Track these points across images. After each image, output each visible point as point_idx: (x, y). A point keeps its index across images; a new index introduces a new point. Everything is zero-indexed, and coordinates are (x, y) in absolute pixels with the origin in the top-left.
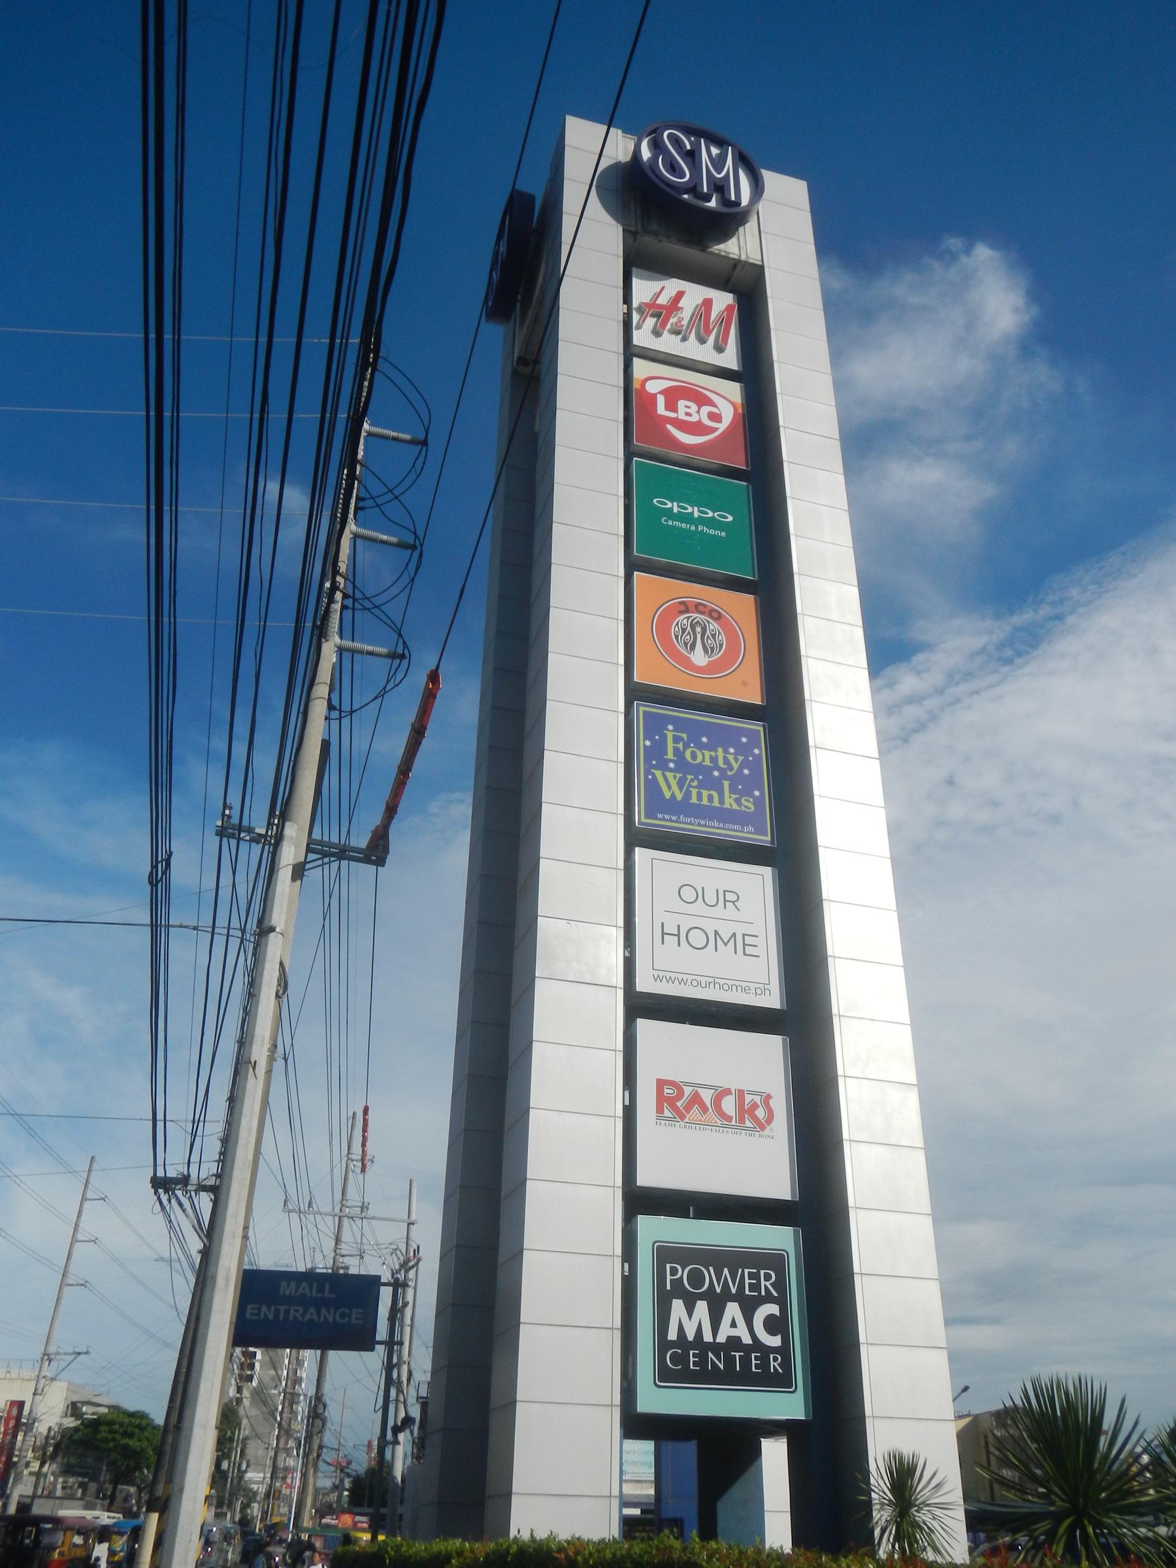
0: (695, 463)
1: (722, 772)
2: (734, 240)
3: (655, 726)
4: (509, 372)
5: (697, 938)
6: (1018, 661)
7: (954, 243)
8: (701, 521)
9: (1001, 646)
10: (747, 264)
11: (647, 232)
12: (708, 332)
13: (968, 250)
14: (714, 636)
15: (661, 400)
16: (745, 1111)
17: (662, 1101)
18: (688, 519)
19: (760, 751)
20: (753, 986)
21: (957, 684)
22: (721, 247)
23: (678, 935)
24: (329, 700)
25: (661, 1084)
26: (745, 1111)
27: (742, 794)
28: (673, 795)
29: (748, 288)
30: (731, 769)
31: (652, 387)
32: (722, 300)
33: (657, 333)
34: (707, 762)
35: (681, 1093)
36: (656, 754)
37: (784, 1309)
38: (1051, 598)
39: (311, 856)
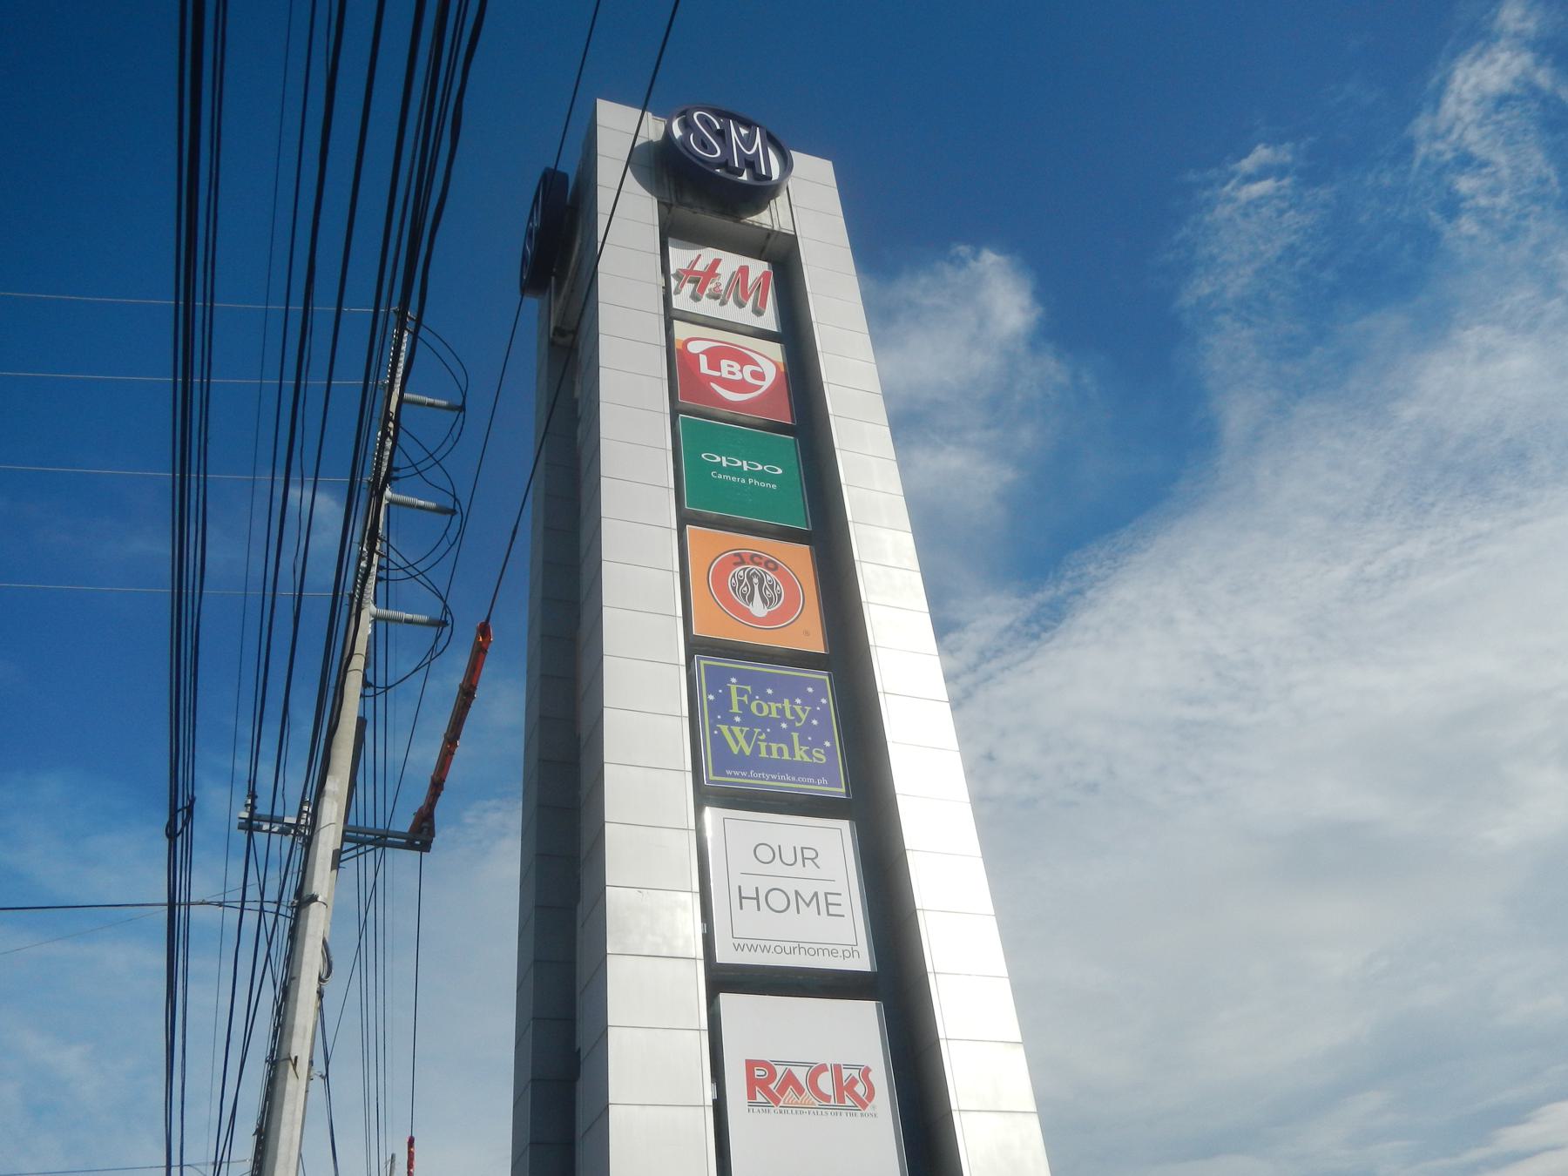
0: (741, 419)
2: (766, 212)
3: (718, 680)
4: (546, 340)
5: (778, 900)
6: (1045, 636)
7: (963, 250)
8: (751, 474)
9: (1027, 622)
11: (681, 204)
12: (747, 297)
13: (976, 256)
14: (772, 587)
15: (703, 360)
16: (844, 1088)
17: (752, 1083)
18: (738, 472)
19: (827, 701)
20: (840, 949)
21: (989, 661)
22: (755, 218)
23: (757, 898)
24: (365, 676)
25: (751, 1065)
26: (844, 1088)
27: (812, 745)
28: (741, 750)
29: (783, 260)
30: (799, 720)
31: (694, 348)
32: (758, 268)
33: (695, 298)
34: (774, 714)
35: (773, 1074)
36: (721, 707)
38: (1070, 574)
39: (347, 846)
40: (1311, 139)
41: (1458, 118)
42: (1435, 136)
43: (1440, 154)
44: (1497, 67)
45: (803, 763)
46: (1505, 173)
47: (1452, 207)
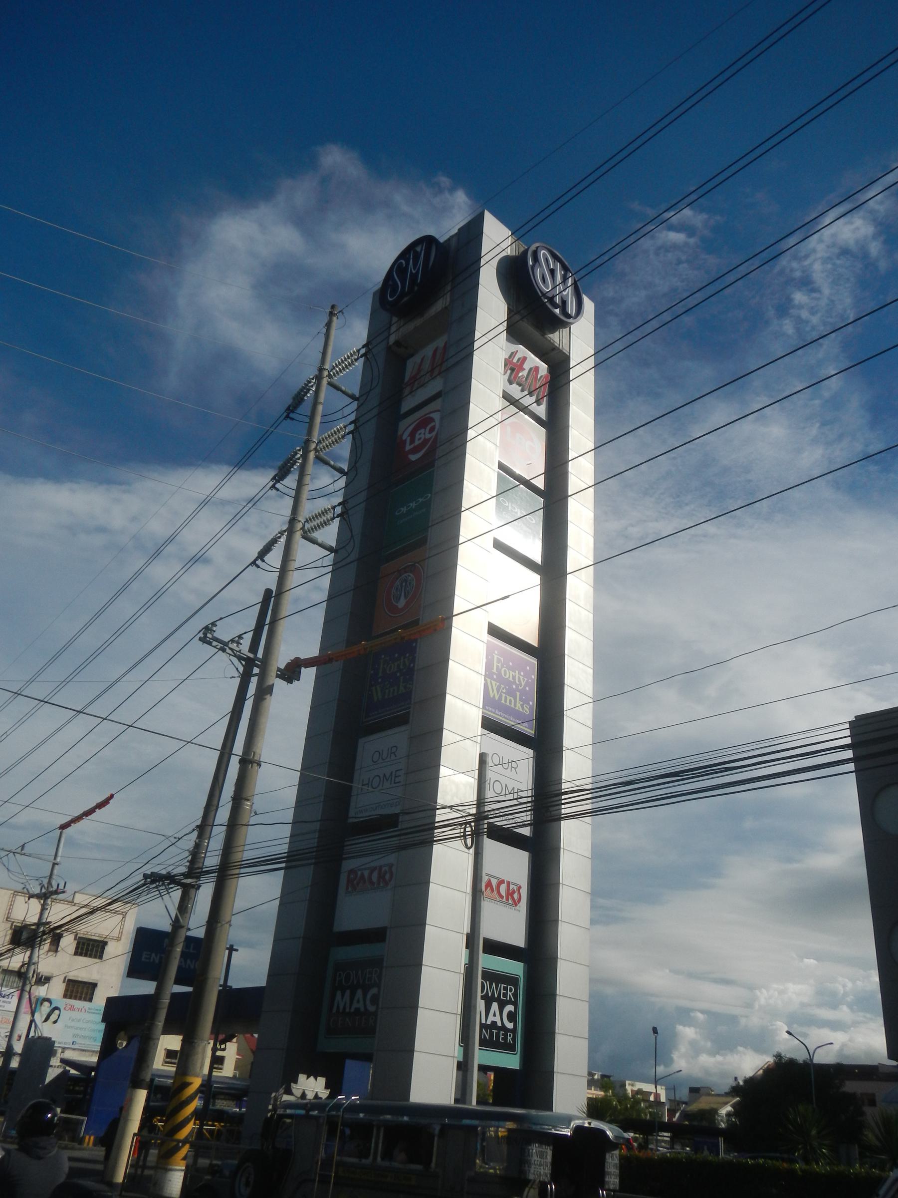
1: (517, 686)
7: (444, 180)
10: (561, 352)
13: (452, 190)
16: (510, 894)
29: (559, 366)
30: (521, 684)
32: (543, 367)
37: (516, 1009)
40: (718, 218)
41: (814, 251)
42: (795, 258)
43: (792, 270)
44: (853, 227)
45: (518, 711)
46: (824, 302)
47: (784, 308)
